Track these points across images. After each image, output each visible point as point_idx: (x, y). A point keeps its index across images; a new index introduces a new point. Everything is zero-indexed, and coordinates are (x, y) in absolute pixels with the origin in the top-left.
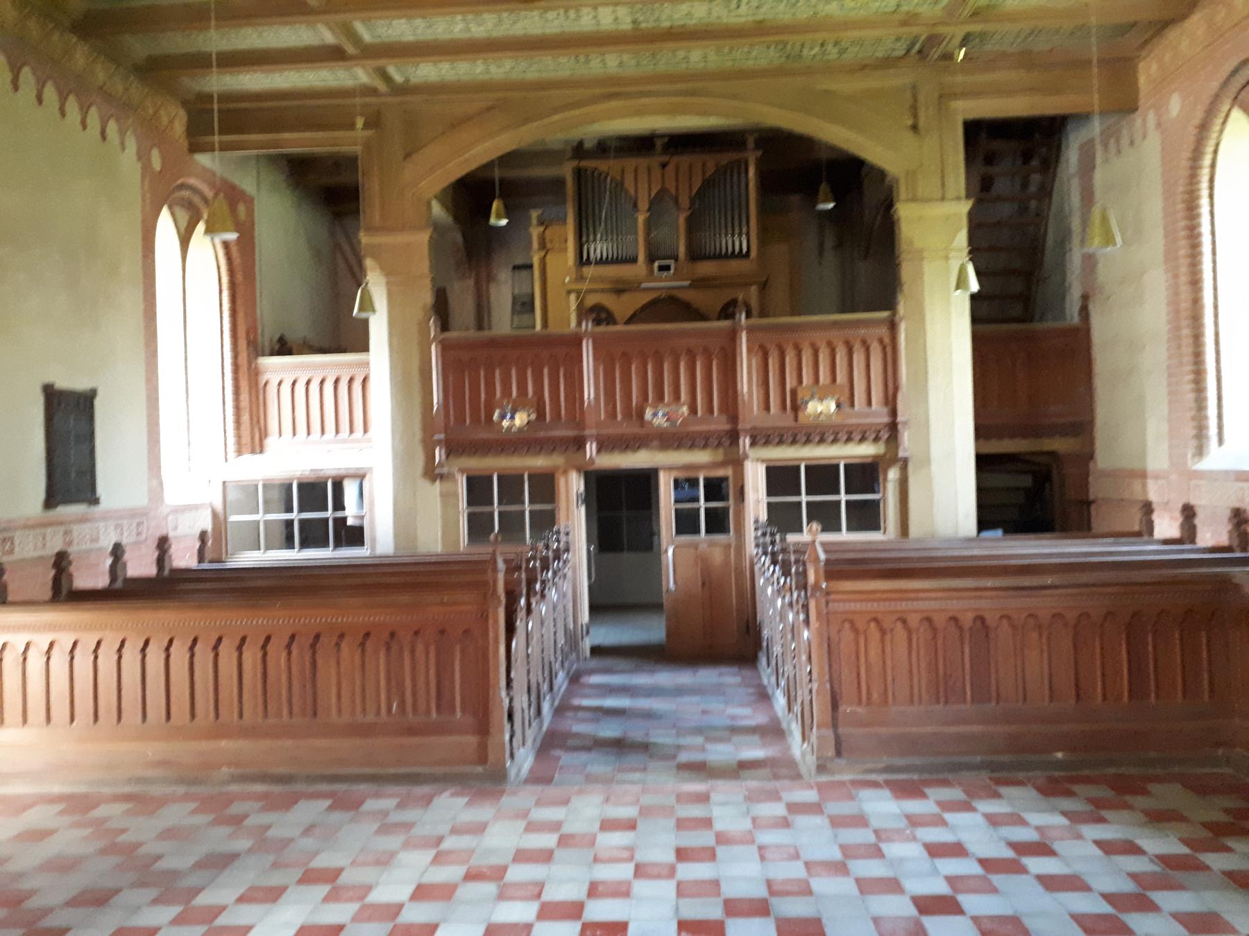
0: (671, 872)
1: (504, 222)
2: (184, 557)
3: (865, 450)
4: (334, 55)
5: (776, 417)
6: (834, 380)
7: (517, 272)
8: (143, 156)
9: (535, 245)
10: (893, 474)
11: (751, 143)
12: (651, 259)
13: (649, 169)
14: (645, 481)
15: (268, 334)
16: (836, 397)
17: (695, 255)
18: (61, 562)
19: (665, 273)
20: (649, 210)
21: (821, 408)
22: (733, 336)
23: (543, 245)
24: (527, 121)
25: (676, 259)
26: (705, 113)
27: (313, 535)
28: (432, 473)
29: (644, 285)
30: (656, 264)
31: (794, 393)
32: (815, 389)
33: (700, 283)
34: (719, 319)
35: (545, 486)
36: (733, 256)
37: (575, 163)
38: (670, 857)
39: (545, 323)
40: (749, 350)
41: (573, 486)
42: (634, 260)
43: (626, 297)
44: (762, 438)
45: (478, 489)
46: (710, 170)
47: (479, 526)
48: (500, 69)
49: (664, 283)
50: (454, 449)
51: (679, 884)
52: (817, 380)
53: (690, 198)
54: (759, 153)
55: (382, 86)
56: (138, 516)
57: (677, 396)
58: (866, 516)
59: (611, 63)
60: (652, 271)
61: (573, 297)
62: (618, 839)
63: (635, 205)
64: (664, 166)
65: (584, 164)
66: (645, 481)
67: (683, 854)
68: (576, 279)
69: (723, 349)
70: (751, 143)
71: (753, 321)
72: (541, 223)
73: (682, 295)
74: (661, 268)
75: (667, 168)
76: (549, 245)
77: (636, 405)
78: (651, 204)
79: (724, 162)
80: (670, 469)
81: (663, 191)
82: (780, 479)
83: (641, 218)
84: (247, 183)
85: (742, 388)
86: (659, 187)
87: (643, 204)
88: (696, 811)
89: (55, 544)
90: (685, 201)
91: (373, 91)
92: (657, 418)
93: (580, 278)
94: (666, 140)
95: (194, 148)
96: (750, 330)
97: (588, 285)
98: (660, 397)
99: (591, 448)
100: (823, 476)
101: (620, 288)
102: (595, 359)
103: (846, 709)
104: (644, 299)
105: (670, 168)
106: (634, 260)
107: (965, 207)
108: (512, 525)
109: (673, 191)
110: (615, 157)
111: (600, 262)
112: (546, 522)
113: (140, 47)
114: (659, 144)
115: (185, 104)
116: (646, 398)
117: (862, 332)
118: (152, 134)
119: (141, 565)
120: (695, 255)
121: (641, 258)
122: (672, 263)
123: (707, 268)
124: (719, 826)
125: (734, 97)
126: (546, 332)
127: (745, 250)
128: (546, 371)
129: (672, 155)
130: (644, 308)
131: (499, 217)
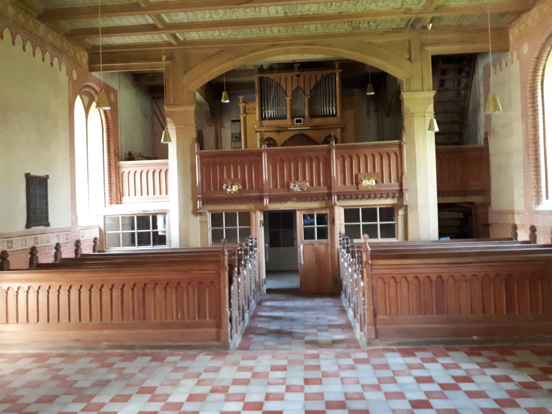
0: (302, 389)
2: (87, 249)
3: (389, 202)
4: (152, 28)
5: (349, 187)
6: (374, 171)
7: (233, 123)
8: (69, 74)
10: (401, 212)
11: (337, 66)
12: (293, 117)
13: (292, 78)
14: (290, 215)
15: (124, 151)
17: (312, 115)
18: (33, 251)
19: (299, 124)
21: (369, 183)
22: (329, 151)
23: (245, 112)
24: (238, 57)
25: (304, 117)
27: (143, 240)
28: (196, 212)
30: (295, 119)
31: (356, 176)
33: (315, 128)
34: (323, 144)
35: (246, 218)
36: (330, 116)
37: (259, 75)
38: (302, 383)
39: (246, 146)
41: (258, 218)
42: (285, 118)
44: (342, 196)
45: (216, 219)
46: (319, 77)
47: (217, 236)
48: (227, 34)
49: (299, 127)
50: (206, 201)
51: (306, 394)
54: (341, 70)
55: (173, 42)
56: (66, 231)
57: (304, 178)
58: (389, 231)
59: (276, 31)
60: (293, 123)
62: (279, 374)
64: (298, 76)
65: (263, 75)
66: (290, 215)
67: (307, 381)
68: (260, 126)
70: (337, 66)
71: (337, 145)
74: (297, 121)
75: (299, 78)
76: (247, 112)
79: (326, 74)
80: (301, 210)
81: (298, 87)
82: (351, 214)
83: (288, 99)
84: (114, 84)
87: (289, 93)
88: (313, 362)
89: (30, 244)
90: (308, 92)
91: (170, 44)
92: (295, 187)
93: (262, 126)
95: (92, 70)
96: (337, 148)
98: (297, 179)
99: (266, 201)
100: (369, 213)
101: (279, 130)
102: (268, 162)
103: (380, 317)
104: (289, 135)
105: (301, 78)
106: (285, 118)
107: (432, 94)
108: (231, 235)
111: (271, 119)
112: (246, 234)
113: (68, 25)
114: (296, 66)
115: (87, 50)
117: (387, 149)
118: (73, 63)
119: (68, 253)
120: (312, 115)
121: (289, 117)
122: (302, 119)
123: (317, 121)
124: (323, 369)
125: (329, 45)
130: (289, 139)
131: (225, 99)
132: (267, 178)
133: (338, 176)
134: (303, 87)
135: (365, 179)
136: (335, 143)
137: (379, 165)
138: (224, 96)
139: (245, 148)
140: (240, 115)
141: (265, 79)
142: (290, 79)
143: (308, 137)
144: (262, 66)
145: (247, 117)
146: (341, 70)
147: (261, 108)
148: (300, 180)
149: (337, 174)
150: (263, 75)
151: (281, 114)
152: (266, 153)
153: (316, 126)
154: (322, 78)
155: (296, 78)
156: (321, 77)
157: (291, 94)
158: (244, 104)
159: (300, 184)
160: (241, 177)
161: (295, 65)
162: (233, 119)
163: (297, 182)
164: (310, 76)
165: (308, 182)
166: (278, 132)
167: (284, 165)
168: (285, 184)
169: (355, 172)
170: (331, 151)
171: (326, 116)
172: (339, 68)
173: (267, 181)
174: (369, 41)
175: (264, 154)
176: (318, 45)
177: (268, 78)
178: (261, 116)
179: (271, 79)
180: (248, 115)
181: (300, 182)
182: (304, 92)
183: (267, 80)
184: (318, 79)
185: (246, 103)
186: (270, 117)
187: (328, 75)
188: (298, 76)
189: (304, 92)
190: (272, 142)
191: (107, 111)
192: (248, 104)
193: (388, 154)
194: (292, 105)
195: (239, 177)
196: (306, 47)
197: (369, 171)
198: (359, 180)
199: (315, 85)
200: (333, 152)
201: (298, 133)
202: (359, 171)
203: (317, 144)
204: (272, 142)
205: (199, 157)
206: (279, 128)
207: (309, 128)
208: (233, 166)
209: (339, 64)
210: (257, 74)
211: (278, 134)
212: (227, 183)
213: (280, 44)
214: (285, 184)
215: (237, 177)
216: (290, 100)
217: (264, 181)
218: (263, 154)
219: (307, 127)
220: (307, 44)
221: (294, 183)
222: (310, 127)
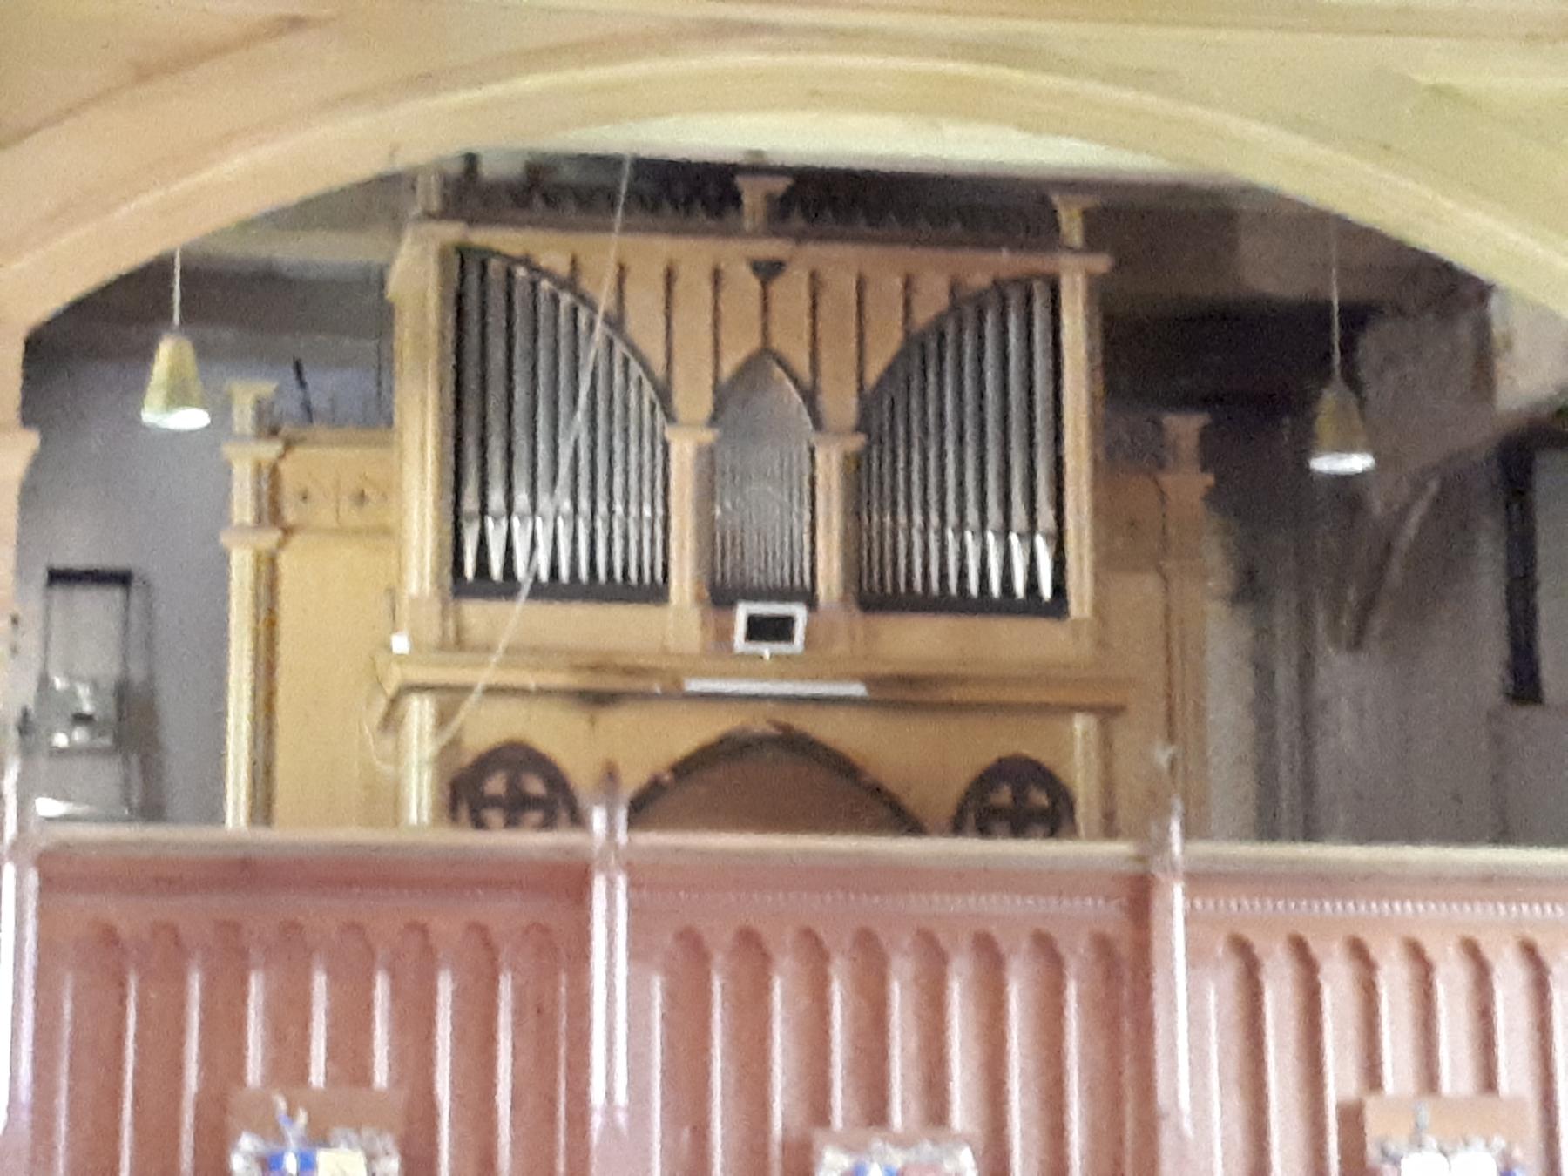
1: (193, 419)
6: (1488, 1081)
7: (59, 593)
9: (243, 508)
11: (1072, 226)
12: (720, 596)
13: (717, 277)
16: (1499, 1142)
19: (766, 649)
20: (714, 420)
23: (271, 511)
24: (425, 82)
25: (810, 599)
26: (1032, 124)
29: (694, 685)
30: (743, 611)
31: (1352, 1118)
32: (1426, 1114)
34: (957, 827)
36: (1007, 605)
37: (452, 232)
39: (263, 807)
40: (1196, 956)
42: (655, 593)
43: (619, 722)
46: (932, 300)
52: (1429, 1079)
53: (716, 388)
54: (1101, 263)
57: (936, 1111)
60: (725, 635)
61: (420, 712)
63: (664, 395)
64: (768, 271)
65: (482, 237)
68: (442, 647)
69: (1103, 946)
70: (1072, 226)
71: (1202, 848)
72: (268, 427)
73: (829, 729)
74: (760, 629)
75: (778, 288)
76: (290, 515)
77: (785, 1129)
78: (722, 397)
79: (980, 280)
81: (765, 357)
83: (684, 448)
85: (1175, 1093)
86: (753, 343)
87: (694, 399)
90: (841, 403)
93: (458, 643)
94: (780, 185)
96: (1197, 880)
97: (500, 665)
98: (875, 1112)
102: (634, 955)
105: (791, 292)
106: (655, 593)
109: (801, 363)
110: (626, 229)
111: (551, 589)
114: (753, 193)
116: (820, 1113)
117: (1404, 909)
121: (683, 583)
122: (799, 612)
125: (1143, 78)
126: (264, 835)
127: (1046, 591)
128: (445, 987)
129: (800, 238)
130: (686, 768)
131: (178, 397)
132: (621, 1097)
133: (1206, 1112)
134: (801, 363)
135: (1418, 1144)
136: (1188, 833)
137: (1352, 1034)
138: (173, 372)
139: (253, 819)
140: (225, 539)
141: (494, 264)
142: (706, 289)
143: (842, 767)
144: (471, 160)
145: (285, 561)
146: (1101, 263)
147: (457, 503)
148: (897, 1118)
149: (1200, 1101)
150: (482, 237)
151: (615, 558)
152: (622, 882)
153: (907, 681)
154: (955, 306)
155: (755, 284)
156: (943, 300)
157: (705, 406)
158: (269, 450)
159: (897, 1159)
160: (396, 1081)
161: (742, 182)
162: (62, 561)
163: (877, 1144)
164: (908, 284)
165: (969, 1142)
166: (596, 700)
167: (244, 981)
168: (775, 1152)
169: (1340, 1081)
170: (1157, 904)
171: (983, 605)
172: (1093, 243)
173: (622, 1118)
174: (1443, 80)
175: (611, 885)
176: (1069, 67)
177: (526, 261)
178: (449, 558)
179: (547, 274)
180: (296, 541)
181: (903, 1143)
182: (810, 397)
183: (510, 275)
184: (924, 315)
185: (289, 445)
186: (544, 575)
187: (997, 285)
188: (768, 271)
189: (810, 397)
190: (1040, 799)
191: (263, 465)
192: (299, 452)
193: (1300, 949)
194: (708, 492)
195: (381, 1076)
196: (966, 69)
197: (1446, 1084)
198: (1372, 1152)
199: (903, 355)
200: (1170, 911)
201: (758, 723)
202: (1372, 1075)
203: (909, 824)
204: (1040, 799)
205: (32, 879)
206: (596, 668)
207: (857, 690)
208: (394, 976)
209: (1086, 213)
210: (429, 216)
211: (592, 722)
212: (270, 1130)
213: (774, 29)
214: (775, 1152)
215: (362, 1076)
216: (700, 451)
217: (597, 1121)
218: (599, 885)
219: (837, 678)
220: (976, 51)
221: (848, 1148)
222: (870, 681)
